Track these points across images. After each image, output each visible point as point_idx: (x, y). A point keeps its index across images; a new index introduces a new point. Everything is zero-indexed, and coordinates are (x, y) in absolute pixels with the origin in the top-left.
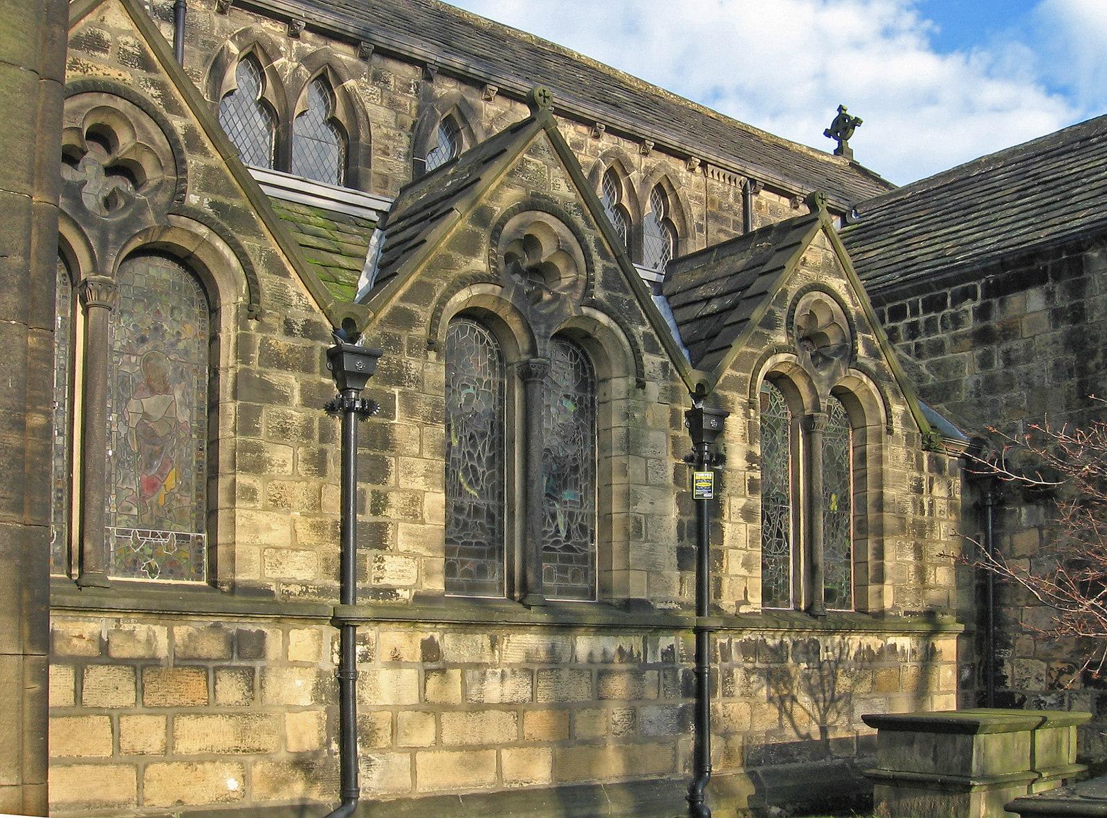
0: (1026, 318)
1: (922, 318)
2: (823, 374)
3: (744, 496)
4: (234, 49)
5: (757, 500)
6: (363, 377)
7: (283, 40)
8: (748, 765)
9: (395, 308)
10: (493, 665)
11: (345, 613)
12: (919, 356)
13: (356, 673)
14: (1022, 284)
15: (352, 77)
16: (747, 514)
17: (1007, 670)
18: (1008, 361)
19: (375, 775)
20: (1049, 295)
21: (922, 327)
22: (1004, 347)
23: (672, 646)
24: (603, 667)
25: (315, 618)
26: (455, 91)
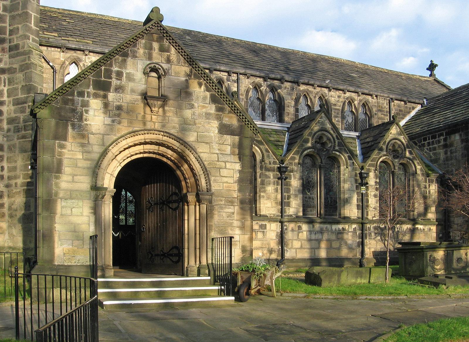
0: (456, 141)
1: (431, 141)
2: (396, 160)
3: (374, 192)
4: (251, 87)
5: (378, 193)
6: (285, 172)
7: (262, 82)
8: (376, 256)
9: (291, 157)
10: (313, 231)
11: (282, 220)
12: (430, 151)
13: (284, 232)
14: (454, 132)
15: (280, 89)
16: (375, 196)
17: (451, 234)
18: (451, 153)
19: (288, 253)
20: (461, 135)
21: (431, 143)
22: (450, 149)
23: (355, 227)
24: (339, 232)
25: (276, 221)
26: (306, 88)
